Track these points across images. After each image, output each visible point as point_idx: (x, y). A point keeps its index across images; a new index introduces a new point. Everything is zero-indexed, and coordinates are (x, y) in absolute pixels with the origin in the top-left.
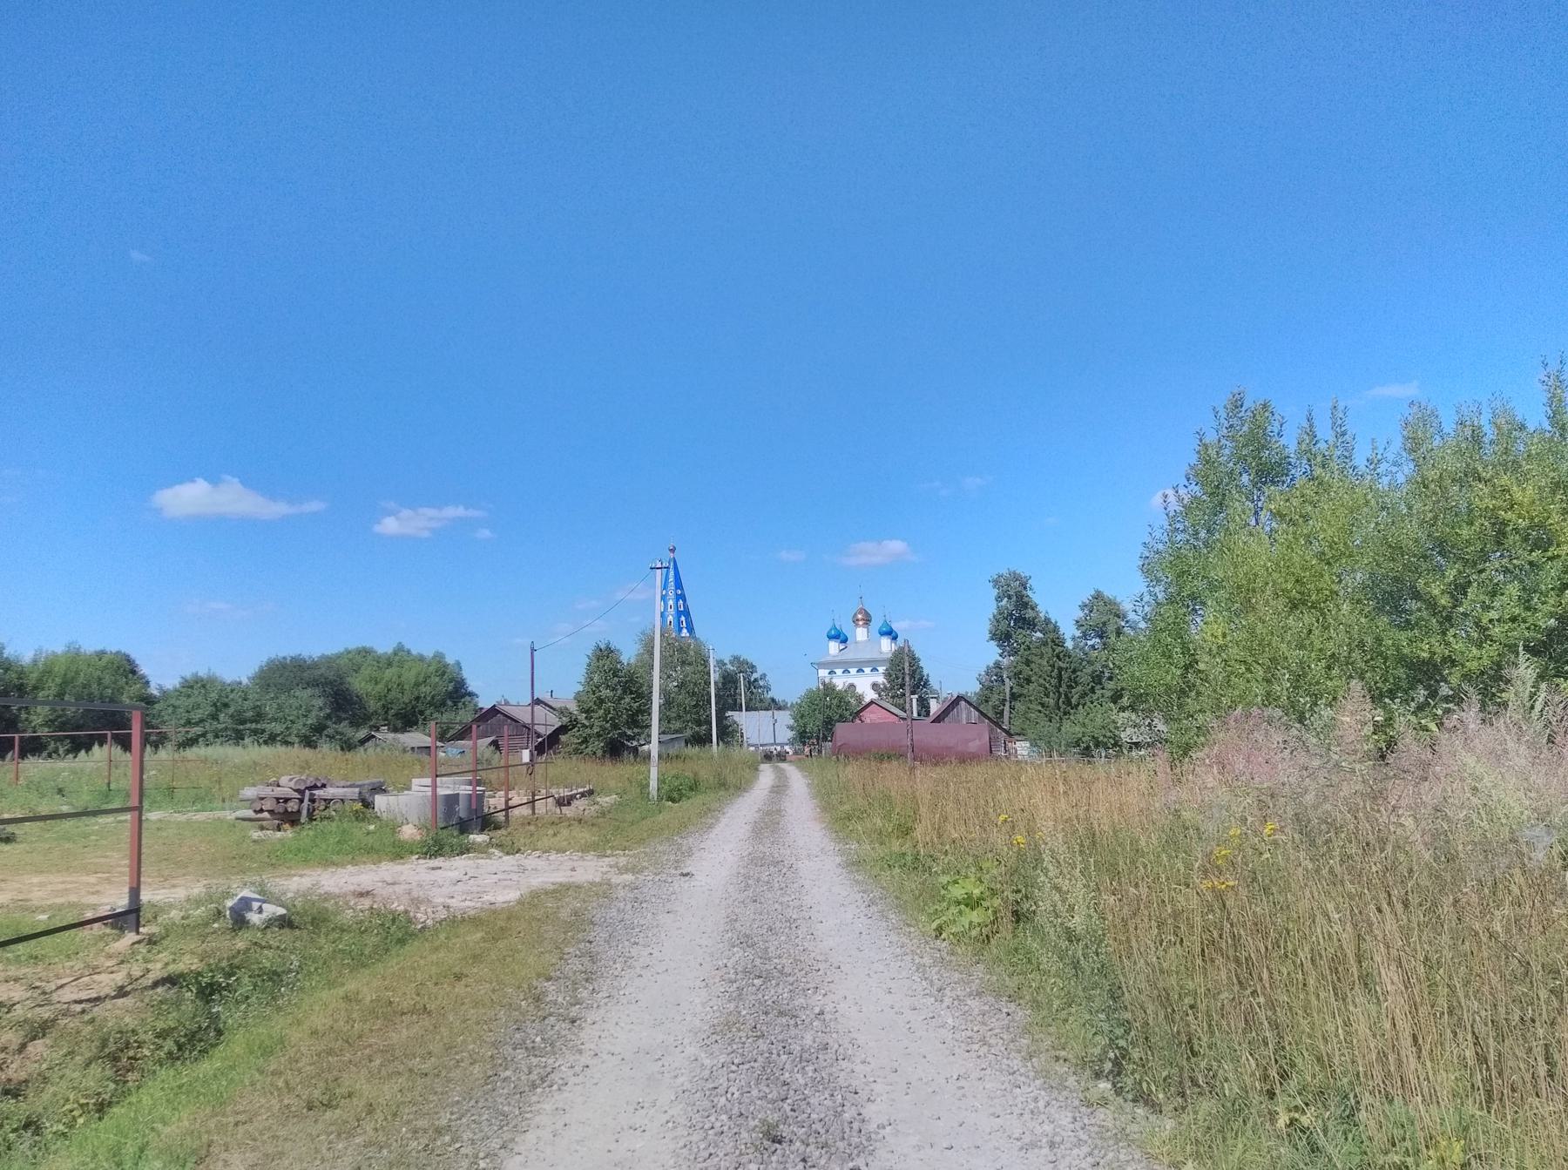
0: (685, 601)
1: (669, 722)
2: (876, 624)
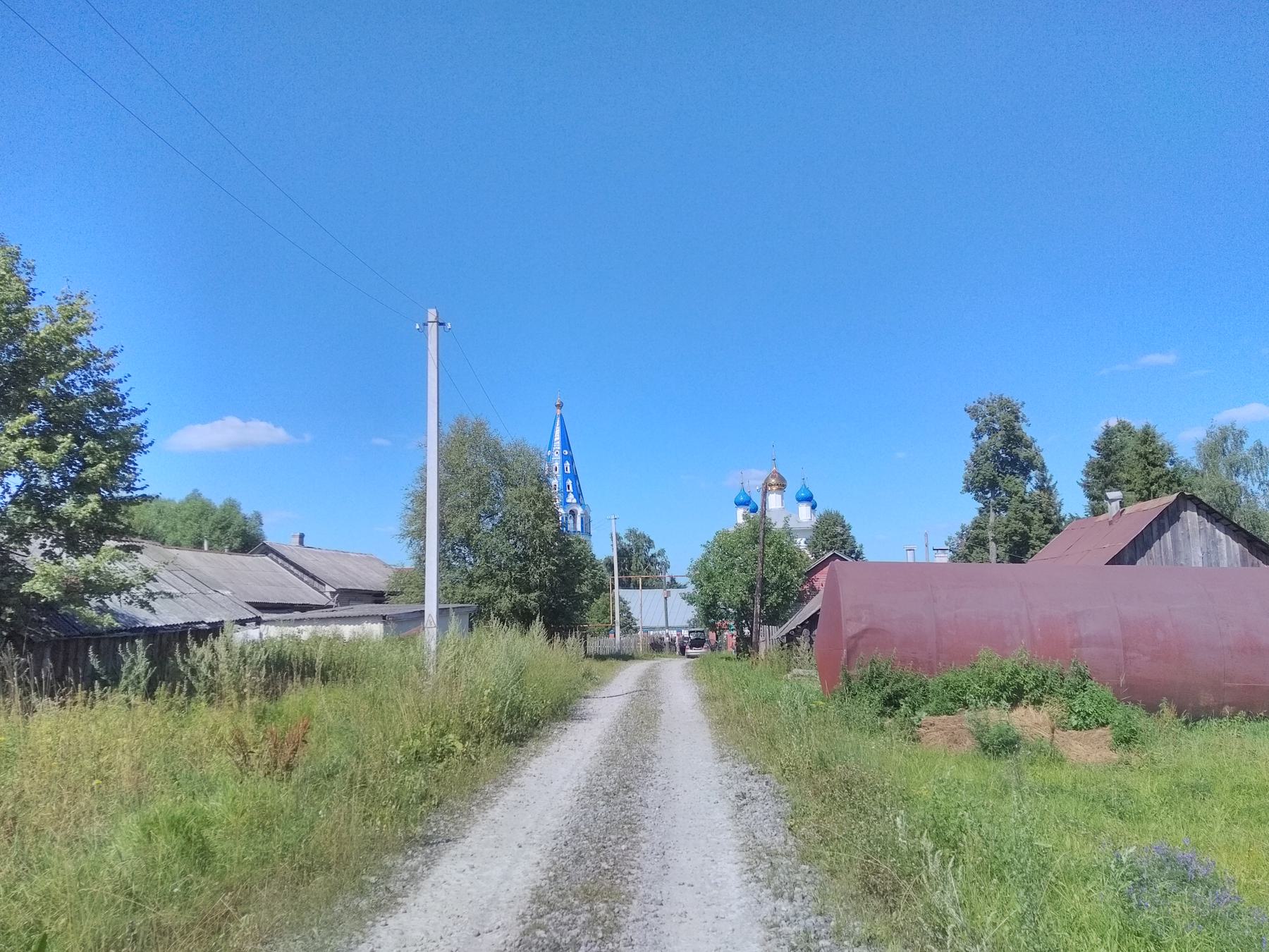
0: (572, 462)
1: (470, 585)
2: (793, 488)
